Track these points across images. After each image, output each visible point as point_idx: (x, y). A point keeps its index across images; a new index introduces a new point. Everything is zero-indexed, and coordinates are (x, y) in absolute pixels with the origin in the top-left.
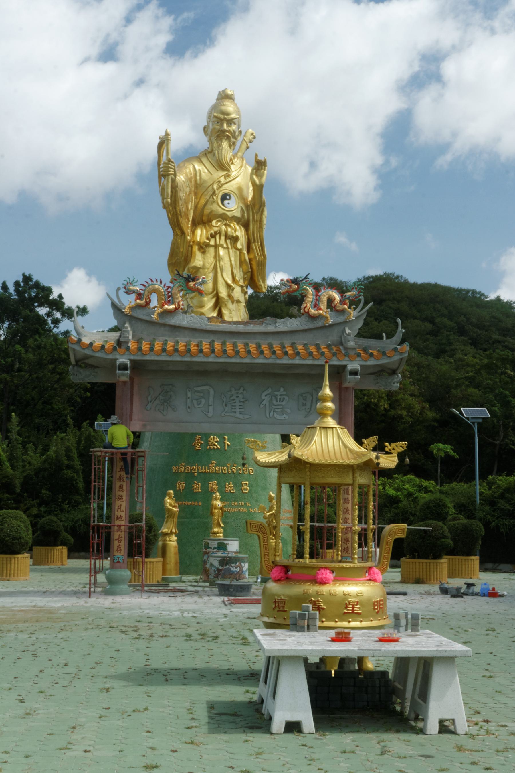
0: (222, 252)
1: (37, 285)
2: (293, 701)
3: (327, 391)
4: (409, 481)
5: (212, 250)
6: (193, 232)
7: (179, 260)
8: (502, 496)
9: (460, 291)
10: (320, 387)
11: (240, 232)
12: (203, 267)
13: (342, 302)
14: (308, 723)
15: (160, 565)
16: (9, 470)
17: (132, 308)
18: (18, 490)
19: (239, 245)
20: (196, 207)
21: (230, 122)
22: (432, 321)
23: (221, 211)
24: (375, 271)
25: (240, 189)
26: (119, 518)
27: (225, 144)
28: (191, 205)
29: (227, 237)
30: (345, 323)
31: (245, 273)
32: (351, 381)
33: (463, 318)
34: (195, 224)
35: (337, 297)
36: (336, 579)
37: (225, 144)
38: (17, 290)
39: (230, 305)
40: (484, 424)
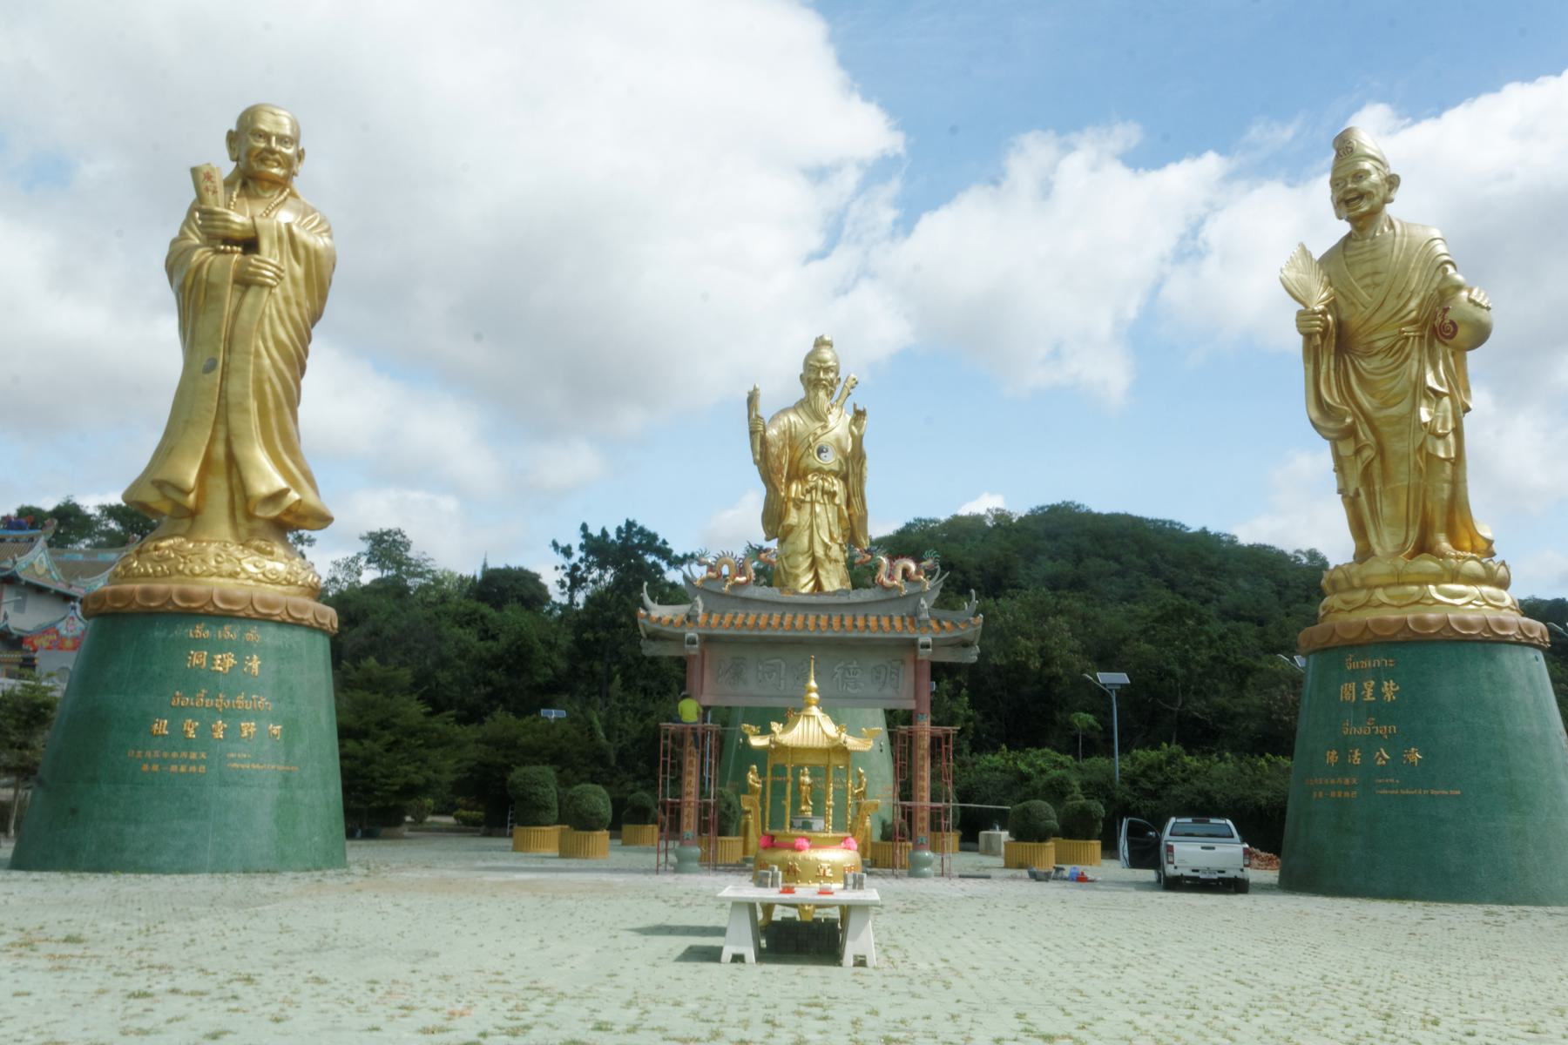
0: (818, 508)
1: (642, 531)
2: (741, 941)
3: (813, 684)
4: (1044, 755)
5: (808, 506)
6: (788, 487)
7: (774, 519)
8: (1144, 774)
9: (1154, 521)
10: (807, 680)
11: (838, 486)
12: (798, 525)
13: (918, 572)
14: (750, 954)
15: (740, 846)
16: (604, 741)
17: (703, 581)
18: (613, 763)
19: (837, 501)
20: (791, 462)
21: (827, 370)
22: (1117, 559)
23: (817, 465)
24: (1492, 336)
25: (838, 440)
26: (689, 794)
27: (822, 394)
28: (785, 460)
29: (824, 492)
30: (921, 593)
31: (844, 530)
32: (924, 654)
33: (1156, 555)
34: (790, 480)
35: (912, 567)
36: (811, 847)
37: (822, 394)
38: (619, 537)
39: (827, 565)
40: (1123, 691)
